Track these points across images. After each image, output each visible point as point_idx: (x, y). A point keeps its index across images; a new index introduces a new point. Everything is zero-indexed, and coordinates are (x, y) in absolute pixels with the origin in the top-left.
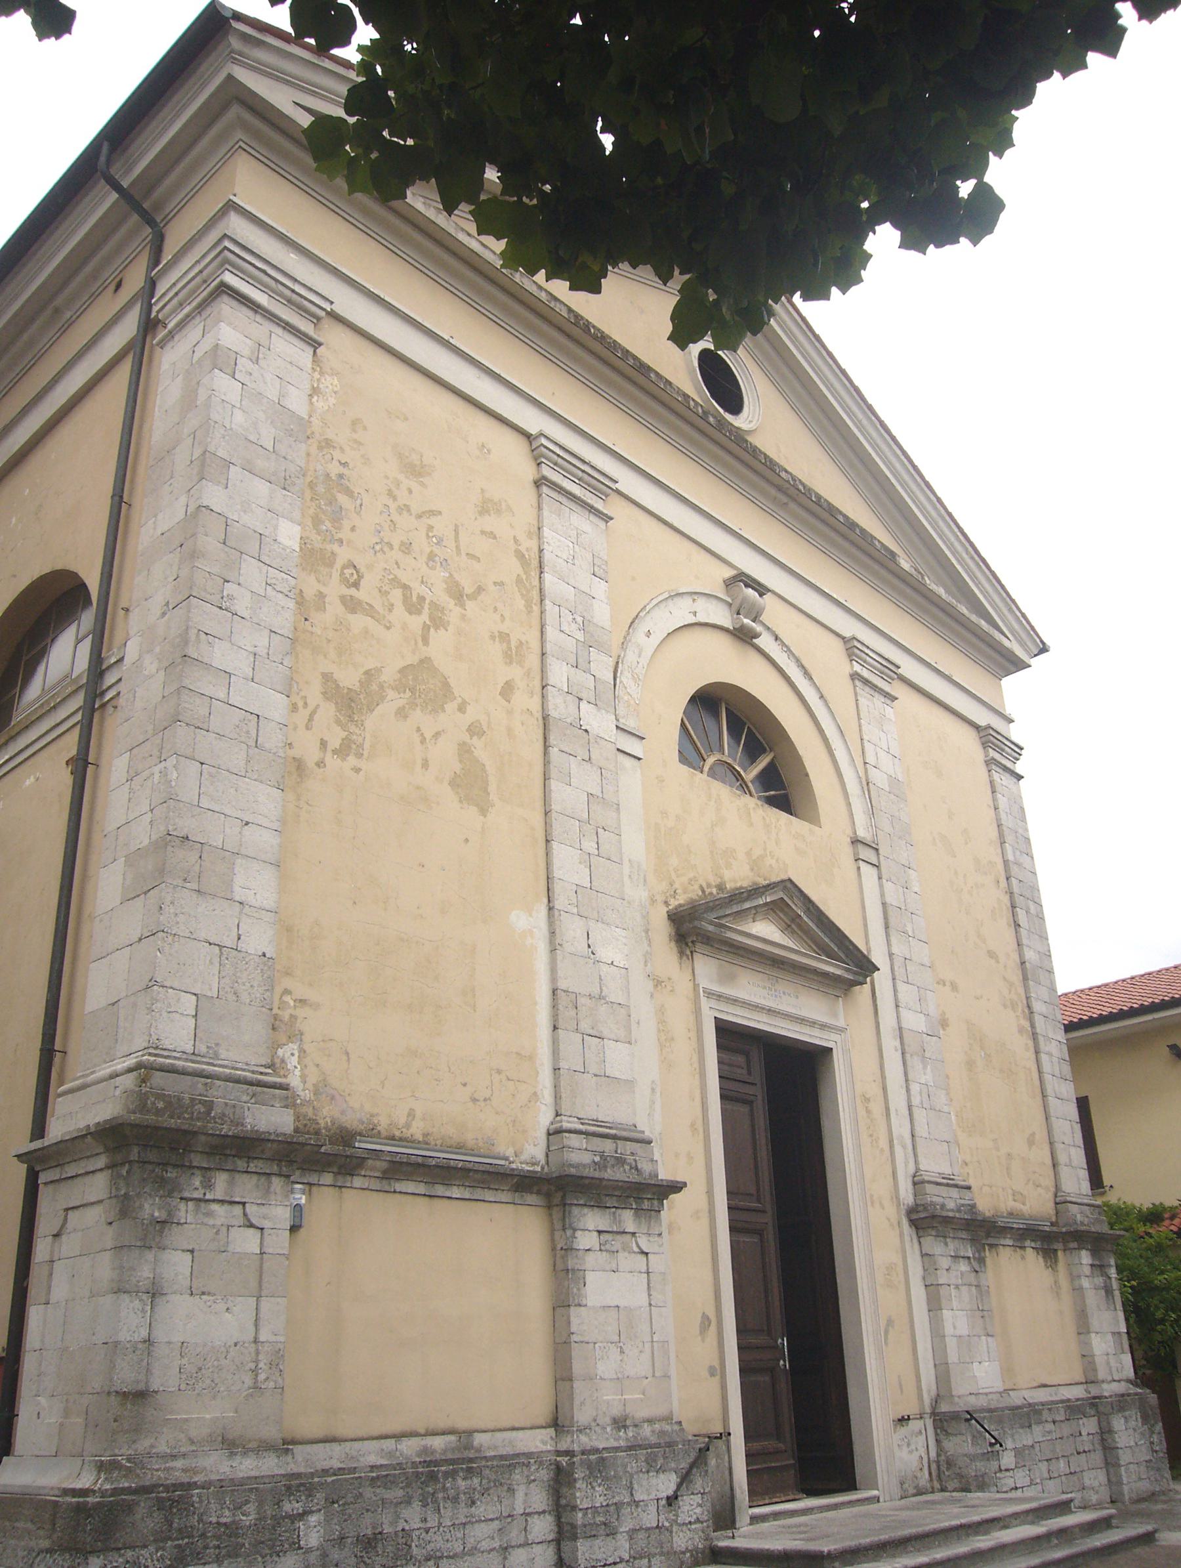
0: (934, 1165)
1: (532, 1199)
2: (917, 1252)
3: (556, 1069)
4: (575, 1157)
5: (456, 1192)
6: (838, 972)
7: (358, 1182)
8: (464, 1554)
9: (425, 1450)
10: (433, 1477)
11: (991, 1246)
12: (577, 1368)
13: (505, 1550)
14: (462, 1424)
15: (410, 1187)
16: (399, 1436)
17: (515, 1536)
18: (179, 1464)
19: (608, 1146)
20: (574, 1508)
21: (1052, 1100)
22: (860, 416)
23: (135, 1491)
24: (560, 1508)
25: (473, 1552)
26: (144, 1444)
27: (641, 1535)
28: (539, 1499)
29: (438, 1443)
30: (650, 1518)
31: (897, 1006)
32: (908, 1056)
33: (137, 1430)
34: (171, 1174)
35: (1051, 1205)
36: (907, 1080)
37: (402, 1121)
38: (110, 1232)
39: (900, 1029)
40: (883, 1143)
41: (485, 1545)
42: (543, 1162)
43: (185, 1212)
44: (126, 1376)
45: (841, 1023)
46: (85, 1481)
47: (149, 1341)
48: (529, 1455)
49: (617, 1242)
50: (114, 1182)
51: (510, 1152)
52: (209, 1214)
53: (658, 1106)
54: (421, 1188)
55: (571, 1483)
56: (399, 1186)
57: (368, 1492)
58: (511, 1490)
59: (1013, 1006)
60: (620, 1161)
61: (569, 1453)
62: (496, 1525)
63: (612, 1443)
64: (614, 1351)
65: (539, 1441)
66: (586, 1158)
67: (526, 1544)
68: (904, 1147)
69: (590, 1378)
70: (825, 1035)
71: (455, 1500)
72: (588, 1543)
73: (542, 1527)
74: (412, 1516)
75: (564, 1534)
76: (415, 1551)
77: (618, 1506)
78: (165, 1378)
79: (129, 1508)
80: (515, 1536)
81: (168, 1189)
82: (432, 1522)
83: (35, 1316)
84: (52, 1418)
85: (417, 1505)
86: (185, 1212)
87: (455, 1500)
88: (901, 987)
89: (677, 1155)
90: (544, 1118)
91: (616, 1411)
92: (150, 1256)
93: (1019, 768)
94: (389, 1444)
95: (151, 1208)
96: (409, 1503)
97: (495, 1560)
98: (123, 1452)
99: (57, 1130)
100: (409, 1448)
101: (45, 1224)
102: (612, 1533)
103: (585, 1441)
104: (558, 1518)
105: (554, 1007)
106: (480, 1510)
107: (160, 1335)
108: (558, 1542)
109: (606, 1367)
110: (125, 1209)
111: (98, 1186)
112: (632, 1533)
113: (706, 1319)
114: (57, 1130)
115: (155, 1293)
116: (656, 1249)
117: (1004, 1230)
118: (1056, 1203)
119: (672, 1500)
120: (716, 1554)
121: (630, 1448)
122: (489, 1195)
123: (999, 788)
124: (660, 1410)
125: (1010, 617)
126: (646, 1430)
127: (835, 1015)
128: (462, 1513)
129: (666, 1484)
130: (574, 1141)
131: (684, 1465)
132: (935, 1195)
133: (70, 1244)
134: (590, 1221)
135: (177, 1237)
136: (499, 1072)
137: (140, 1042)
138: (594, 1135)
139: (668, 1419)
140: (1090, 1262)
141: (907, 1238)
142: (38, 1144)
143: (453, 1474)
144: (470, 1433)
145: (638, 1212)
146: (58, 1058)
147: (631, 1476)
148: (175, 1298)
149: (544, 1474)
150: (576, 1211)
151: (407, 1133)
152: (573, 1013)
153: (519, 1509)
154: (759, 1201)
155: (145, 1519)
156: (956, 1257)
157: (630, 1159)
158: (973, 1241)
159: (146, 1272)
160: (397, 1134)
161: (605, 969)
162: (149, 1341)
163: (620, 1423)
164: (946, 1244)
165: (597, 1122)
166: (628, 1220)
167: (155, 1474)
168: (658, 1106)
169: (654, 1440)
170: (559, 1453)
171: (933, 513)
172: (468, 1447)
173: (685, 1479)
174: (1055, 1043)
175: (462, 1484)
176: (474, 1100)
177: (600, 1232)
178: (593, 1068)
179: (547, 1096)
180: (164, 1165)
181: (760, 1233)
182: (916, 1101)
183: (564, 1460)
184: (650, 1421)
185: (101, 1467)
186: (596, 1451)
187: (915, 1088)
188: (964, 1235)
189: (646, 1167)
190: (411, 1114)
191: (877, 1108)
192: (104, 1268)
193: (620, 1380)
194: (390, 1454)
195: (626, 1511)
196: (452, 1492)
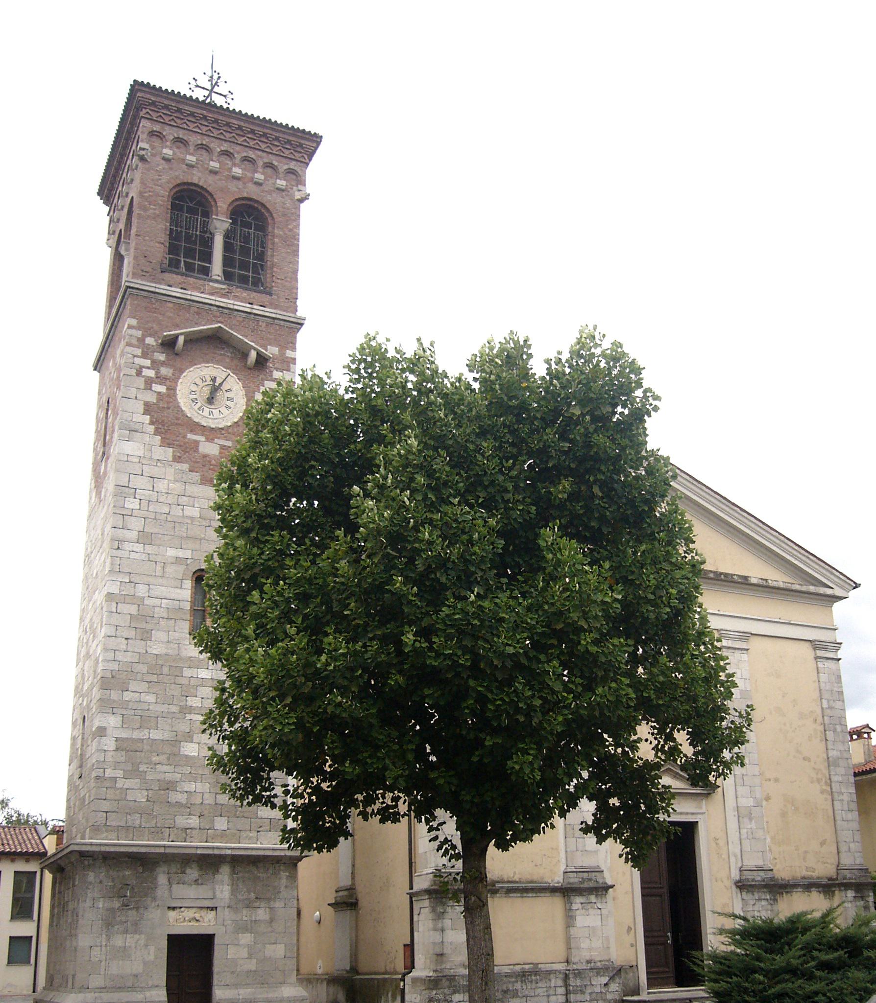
0: (752, 862)
1: (556, 894)
2: (740, 899)
3: (566, 852)
4: (571, 881)
5: (530, 895)
6: (699, 792)
7: (498, 895)
8: (535, 996)
9: (523, 968)
10: (524, 976)
11: (787, 892)
12: (573, 945)
13: (548, 996)
14: (536, 962)
15: (515, 895)
16: (514, 965)
17: (551, 992)
18: (452, 971)
19: (585, 875)
20: (570, 985)
21: (839, 823)
22: (727, 509)
23: (443, 976)
24: (566, 985)
25: (538, 995)
26: (443, 966)
27: (594, 994)
28: (560, 982)
29: (527, 967)
30: (598, 989)
31: (736, 797)
32: (741, 818)
33: (442, 962)
34: (444, 900)
35: (835, 870)
36: (739, 828)
37: (512, 876)
38: (431, 915)
39: (737, 807)
40: (725, 856)
41: (541, 994)
42: (562, 881)
43: (449, 909)
44: (438, 951)
45: (704, 810)
46: (431, 974)
47: (442, 942)
48: (556, 971)
49: (589, 906)
50: (430, 902)
51: (550, 881)
52: (456, 909)
53: (609, 857)
54: (519, 895)
55: (569, 979)
56: (511, 895)
57: (505, 979)
58: (550, 980)
59: (819, 781)
60: (590, 880)
61: (569, 970)
62: (545, 989)
63: (585, 968)
64: (588, 941)
65: (562, 967)
66: (576, 880)
67: (555, 995)
68: (735, 856)
69: (578, 948)
70: (694, 816)
71: (531, 982)
72: (574, 995)
73: (561, 991)
74: (518, 986)
75: (567, 993)
76: (519, 994)
77: (585, 986)
78: (447, 951)
79: (441, 980)
80: (551, 992)
81: (444, 904)
82: (524, 987)
83: (416, 934)
84: (423, 960)
85: (519, 983)
86: (449, 909)
87: (531, 982)
88: (739, 788)
89: (618, 873)
90: (563, 868)
91: (588, 958)
92: (440, 921)
93: (840, 654)
94: (512, 967)
95: (440, 909)
96: (517, 982)
97: (545, 999)
98: (439, 968)
99: (416, 888)
100: (518, 968)
101: (416, 912)
102: (582, 992)
103: (575, 967)
104: (566, 988)
105: (565, 830)
106: (540, 985)
107: (445, 940)
108: (566, 995)
109: (585, 944)
110: (434, 910)
111: (426, 903)
112: (591, 994)
113: (630, 929)
114: (416, 888)
115: (443, 930)
116: (604, 907)
117: (834, 885)
118: (837, 870)
119: (606, 985)
120: (623, 1000)
121: (590, 969)
122: (542, 895)
123: (821, 670)
124: (607, 958)
125: (832, 577)
126: (599, 964)
127: (701, 808)
128: (534, 986)
129: (605, 980)
130: (571, 875)
131: (611, 975)
132: (748, 876)
133: (422, 917)
134: (578, 900)
135: (446, 916)
136: (545, 855)
137: (433, 865)
138: (580, 872)
139: (609, 961)
140: (854, 895)
141: (734, 893)
142: (411, 891)
143: (531, 975)
144: (538, 964)
145: (596, 896)
146: (413, 864)
147: (590, 978)
148: (448, 931)
149: (561, 976)
150: (572, 897)
151: (514, 879)
152: (572, 831)
153: (553, 985)
154: (661, 884)
155: (445, 983)
156: (760, 899)
157: (594, 878)
158: (770, 892)
159: (440, 925)
160: (510, 880)
161: (585, 813)
162: (442, 942)
163: (588, 962)
164: (753, 895)
165: (582, 867)
166: (593, 898)
167: (447, 973)
168: (609, 857)
169: (600, 967)
170: (567, 970)
171: (778, 541)
172: (537, 968)
173: (612, 978)
174: (848, 792)
175: (533, 978)
176: (536, 866)
177: (582, 903)
178: (580, 849)
179: (564, 861)
180: (442, 898)
181: (661, 896)
182: (744, 836)
183: (567, 972)
184: (600, 961)
185: (434, 971)
186: (577, 970)
187: (744, 831)
188: (765, 890)
189: (601, 881)
190: (515, 873)
191: (722, 842)
192: (430, 924)
193: (590, 949)
194: (511, 969)
195: (588, 987)
196: (530, 980)
